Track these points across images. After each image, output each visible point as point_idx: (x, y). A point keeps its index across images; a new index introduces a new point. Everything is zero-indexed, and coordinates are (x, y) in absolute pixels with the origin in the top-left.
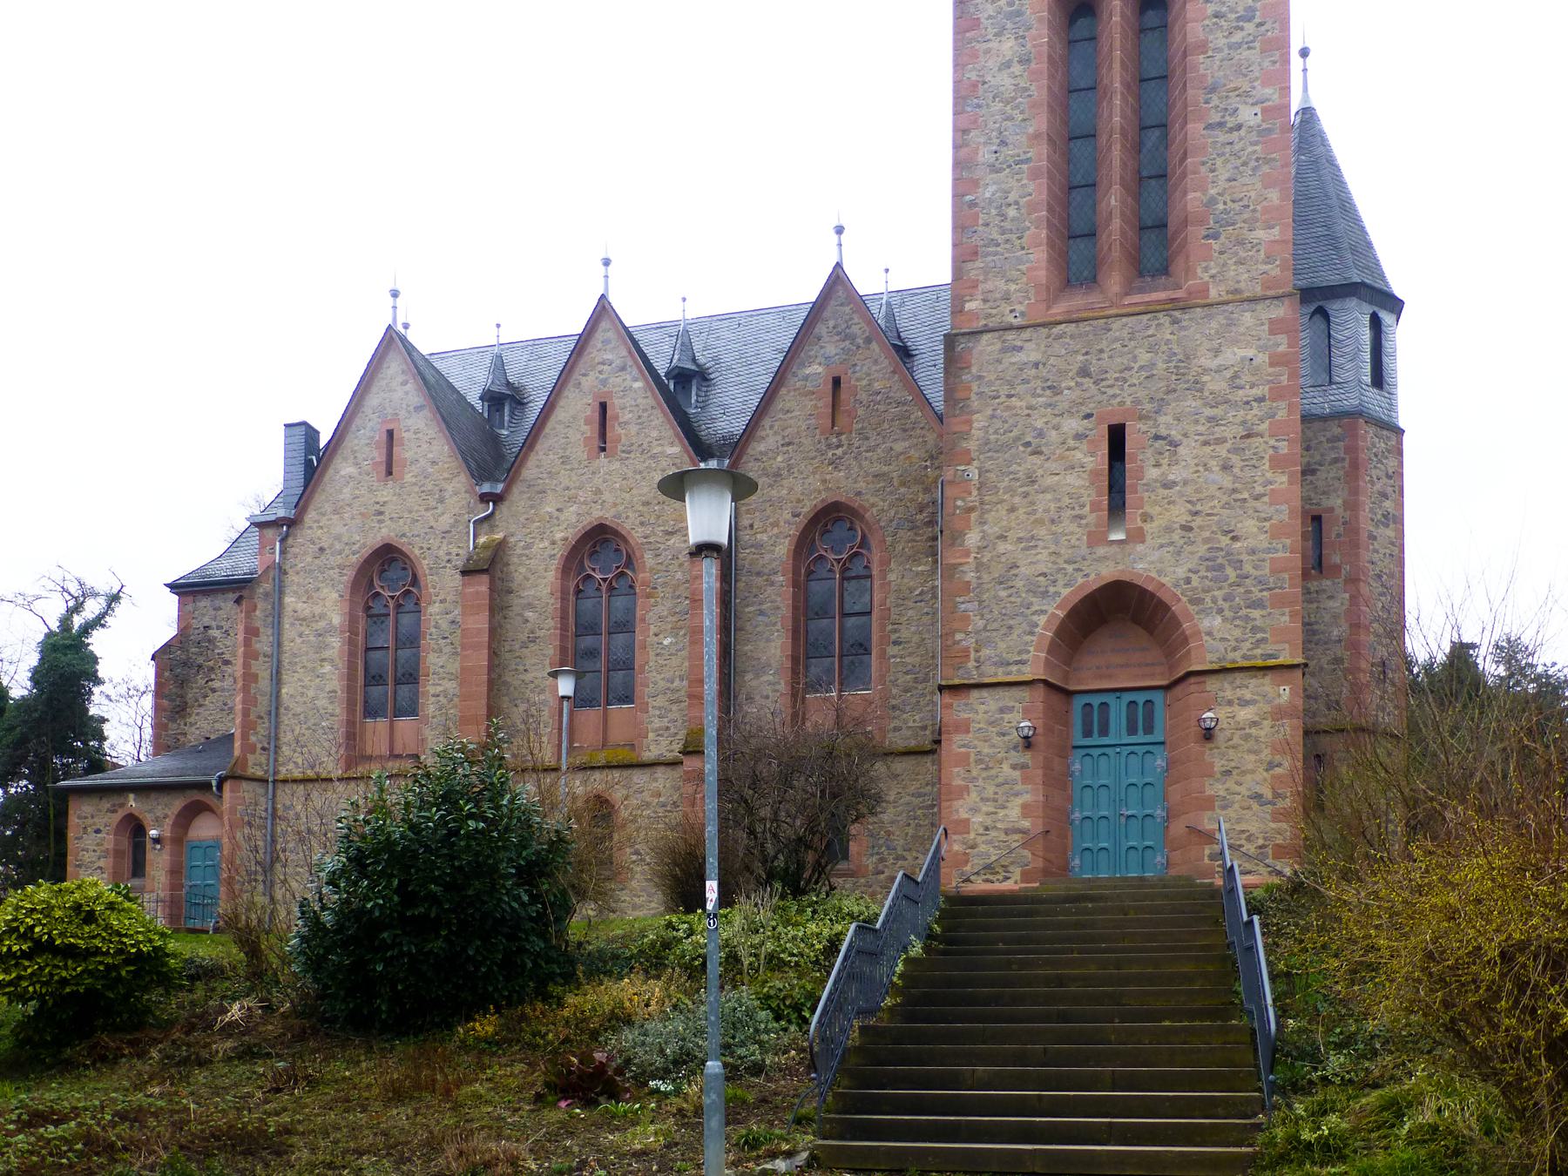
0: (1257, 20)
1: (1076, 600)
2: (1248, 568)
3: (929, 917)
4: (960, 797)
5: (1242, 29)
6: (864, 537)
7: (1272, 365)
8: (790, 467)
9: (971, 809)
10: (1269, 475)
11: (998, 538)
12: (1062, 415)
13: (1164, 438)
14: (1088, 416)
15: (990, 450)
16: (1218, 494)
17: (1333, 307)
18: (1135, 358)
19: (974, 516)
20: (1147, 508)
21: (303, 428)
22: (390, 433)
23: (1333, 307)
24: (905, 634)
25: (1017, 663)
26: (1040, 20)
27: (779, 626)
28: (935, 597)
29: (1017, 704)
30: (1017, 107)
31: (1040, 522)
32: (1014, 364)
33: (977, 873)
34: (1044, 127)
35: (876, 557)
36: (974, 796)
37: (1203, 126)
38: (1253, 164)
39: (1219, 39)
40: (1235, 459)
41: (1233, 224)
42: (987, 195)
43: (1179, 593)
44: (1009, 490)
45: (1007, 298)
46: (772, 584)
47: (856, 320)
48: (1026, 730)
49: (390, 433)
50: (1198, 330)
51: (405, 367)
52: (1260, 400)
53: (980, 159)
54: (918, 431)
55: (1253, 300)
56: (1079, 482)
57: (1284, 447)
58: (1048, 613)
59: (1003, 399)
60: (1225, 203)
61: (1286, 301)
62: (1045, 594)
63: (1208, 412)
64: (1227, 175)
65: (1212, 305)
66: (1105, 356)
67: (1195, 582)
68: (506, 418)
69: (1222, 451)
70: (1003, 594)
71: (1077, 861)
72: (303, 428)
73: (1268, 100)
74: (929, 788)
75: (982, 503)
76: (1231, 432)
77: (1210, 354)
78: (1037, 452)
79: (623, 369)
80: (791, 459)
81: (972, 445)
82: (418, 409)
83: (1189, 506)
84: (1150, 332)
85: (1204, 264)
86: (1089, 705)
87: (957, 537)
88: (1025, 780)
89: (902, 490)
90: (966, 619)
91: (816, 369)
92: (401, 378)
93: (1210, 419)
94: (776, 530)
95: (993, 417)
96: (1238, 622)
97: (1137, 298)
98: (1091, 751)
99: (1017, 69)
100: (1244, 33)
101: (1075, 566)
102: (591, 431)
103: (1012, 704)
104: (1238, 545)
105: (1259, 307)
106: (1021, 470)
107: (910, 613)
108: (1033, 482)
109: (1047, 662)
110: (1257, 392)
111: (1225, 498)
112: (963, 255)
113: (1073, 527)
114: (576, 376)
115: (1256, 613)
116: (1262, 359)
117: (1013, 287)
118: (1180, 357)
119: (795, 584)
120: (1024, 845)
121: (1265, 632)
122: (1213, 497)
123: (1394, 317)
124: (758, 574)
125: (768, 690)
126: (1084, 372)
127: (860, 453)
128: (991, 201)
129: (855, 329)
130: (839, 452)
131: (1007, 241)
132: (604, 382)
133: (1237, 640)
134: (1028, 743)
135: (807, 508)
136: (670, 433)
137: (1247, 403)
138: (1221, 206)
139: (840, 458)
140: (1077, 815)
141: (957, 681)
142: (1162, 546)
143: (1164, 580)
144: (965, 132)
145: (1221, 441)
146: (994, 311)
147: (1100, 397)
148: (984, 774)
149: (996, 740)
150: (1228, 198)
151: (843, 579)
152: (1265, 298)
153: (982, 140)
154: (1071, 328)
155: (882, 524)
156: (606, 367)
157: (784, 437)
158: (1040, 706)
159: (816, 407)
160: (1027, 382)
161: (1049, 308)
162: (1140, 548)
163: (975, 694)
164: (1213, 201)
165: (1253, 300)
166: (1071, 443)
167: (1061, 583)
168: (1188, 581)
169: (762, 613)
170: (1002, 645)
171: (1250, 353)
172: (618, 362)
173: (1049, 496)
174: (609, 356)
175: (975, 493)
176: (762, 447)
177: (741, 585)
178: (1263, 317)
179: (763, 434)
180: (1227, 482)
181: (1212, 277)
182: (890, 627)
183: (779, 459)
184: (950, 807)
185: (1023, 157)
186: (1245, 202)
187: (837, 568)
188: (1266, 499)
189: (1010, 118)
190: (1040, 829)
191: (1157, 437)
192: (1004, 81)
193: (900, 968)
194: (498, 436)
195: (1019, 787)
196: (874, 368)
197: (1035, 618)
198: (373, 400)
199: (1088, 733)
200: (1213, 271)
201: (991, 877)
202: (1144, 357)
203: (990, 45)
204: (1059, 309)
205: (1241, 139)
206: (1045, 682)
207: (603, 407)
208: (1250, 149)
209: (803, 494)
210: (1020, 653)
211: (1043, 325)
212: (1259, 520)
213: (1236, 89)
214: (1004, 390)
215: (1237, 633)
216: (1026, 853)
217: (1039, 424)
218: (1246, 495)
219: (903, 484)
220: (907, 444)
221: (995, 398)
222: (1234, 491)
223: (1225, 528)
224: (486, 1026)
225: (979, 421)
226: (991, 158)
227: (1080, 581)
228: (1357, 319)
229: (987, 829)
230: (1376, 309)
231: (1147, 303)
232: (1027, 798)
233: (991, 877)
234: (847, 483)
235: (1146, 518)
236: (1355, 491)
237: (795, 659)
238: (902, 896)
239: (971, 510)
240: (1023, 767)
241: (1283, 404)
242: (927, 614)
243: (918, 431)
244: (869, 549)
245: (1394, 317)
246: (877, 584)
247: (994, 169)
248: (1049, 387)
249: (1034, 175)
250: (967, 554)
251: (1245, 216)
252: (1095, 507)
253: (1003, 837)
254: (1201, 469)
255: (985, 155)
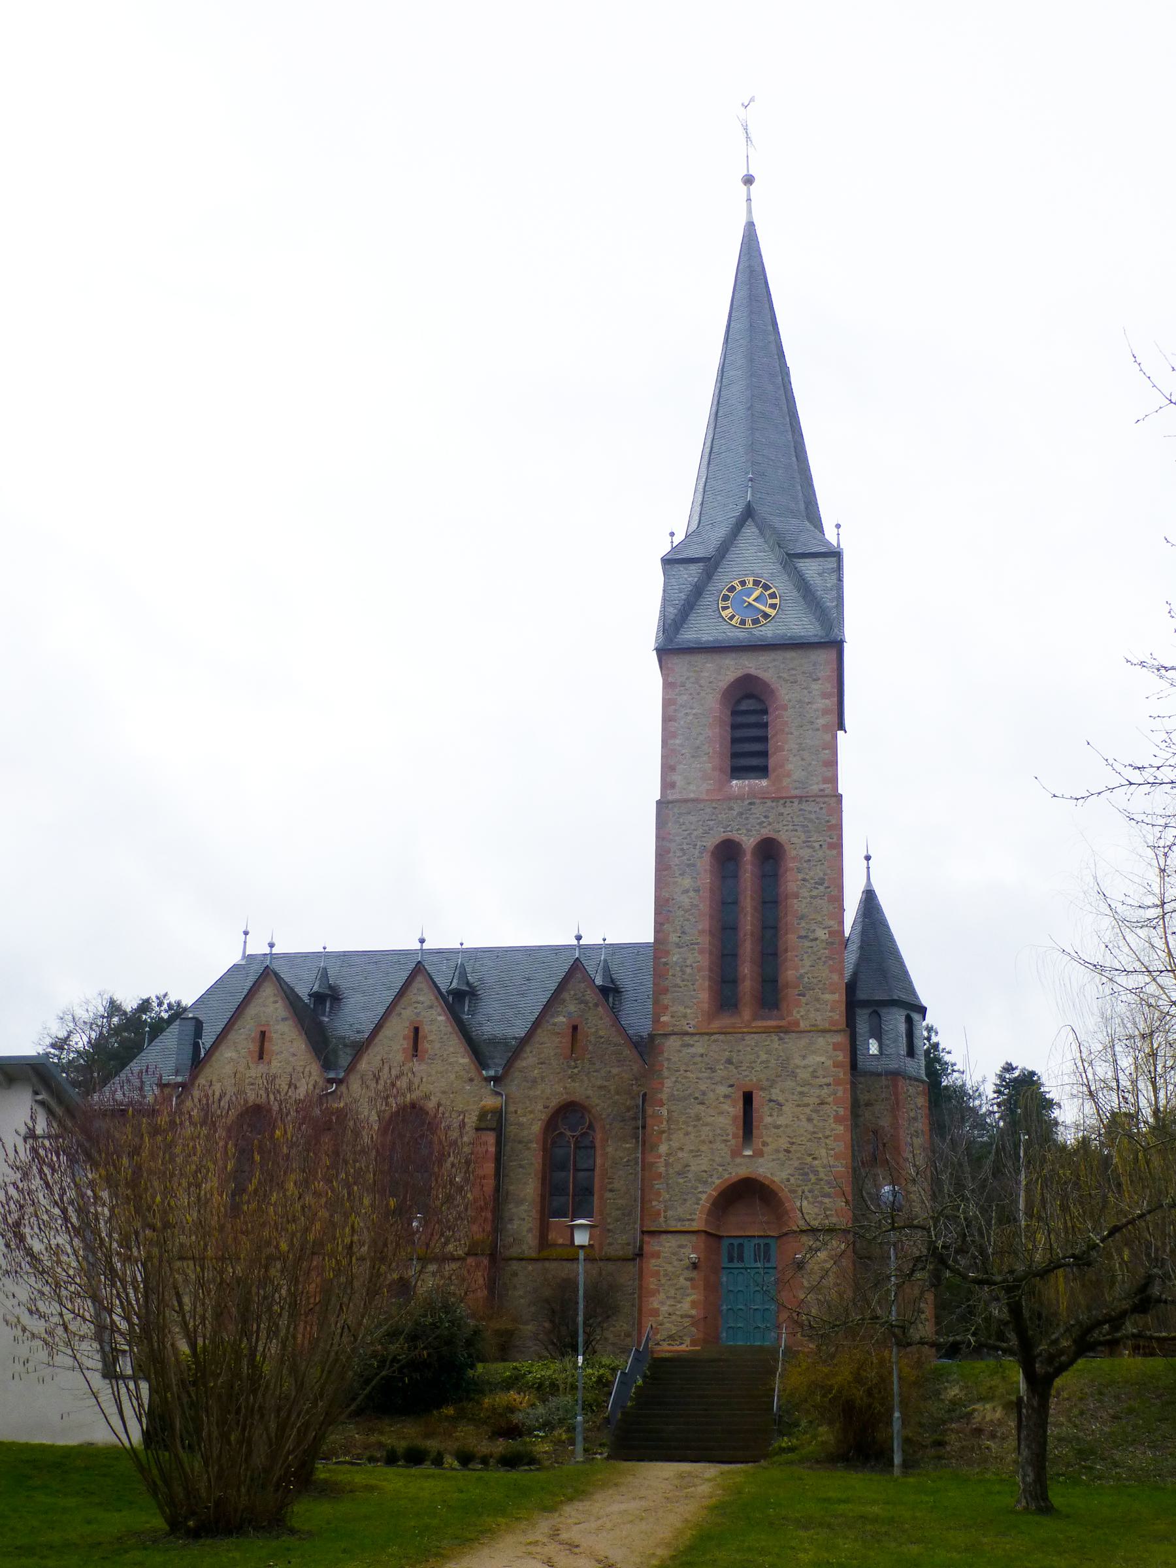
0: (826, 885)
1: (723, 1187)
2: (822, 1175)
3: (645, 1368)
4: (653, 1295)
5: (818, 889)
6: (590, 1123)
7: (834, 1067)
8: (543, 1078)
9: (660, 1303)
10: (833, 1125)
11: (679, 1149)
12: (716, 1084)
13: (774, 1101)
14: (731, 1086)
15: (674, 1100)
16: (805, 1134)
17: (883, 1011)
18: (758, 1057)
19: (664, 1135)
20: (765, 1139)
21: (194, 1021)
22: (263, 1034)
23: (883, 1011)
24: (616, 1185)
25: (689, 1220)
26: (705, 870)
27: (533, 1176)
28: (637, 1163)
29: (688, 1244)
30: (692, 914)
31: (703, 1142)
32: (688, 1053)
33: (664, 1340)
34: (707, 927)
35: (599, 1136)
36: (662, 1296)
37: (796, 936)
38: (823, 959)
39: (804, 892)
40: (814, 1115)
41: (813, 989)
42: (674, 959)
43: (783, 1187)
44: (685, 1123)
45: (685, 1016)
46: (529, 1149)
47: (588, 993)
48: (694, 1259)
49: (263, 1034)
50: (794, 1045)
51: (276, 992)
52: (828, 1085)
53: (671, 940)
54: (628, 1063)
55: (824, 1031)
56: (727, 1122)
57: (841, 1112)
58: (707, 1194)
59: (682, 1072)
60: (809, 978)
61: (842, 1033)
62: (705, 1182)
63: (799, 1089)
64: (809, 964)
65: (801, 1032)
66: (741, 1053)
67: (792, 1180)
68: (327, 1010)
69: (807, 1110)
70: (681, 1181)
71: (724, 1335)
72: (194, 1021)
73: (831, 927)
74: (631, 1282)
75: (669, 1129)
76: (813, 1100)
77: (800, 1058)
78: (702, 1103)
79: (431, 1007)
80: (543, 1072)
81: (664, 1096)
82: (284, 1019)
83: (789, 1139)
84: (767, 1043)
85: (797, 1009)
86: (732, 1244)
87: (654, 1147)
88: (693, 1288)
89: (617, 1097)
90: (658, 1194)
91: (561, 1019)
92: (272, 999)
93: (801, 1093)
94: (532, 1116)
95: (676, 1082)
96: (816, 1204)
97: (759, 1023)
98: (732, 1271)
99: (692, 894)
100: (818, 891)
101: (724, 1168)
102: (407, 1044)
103: (685, 1243)
104: (817, 1162)
105: (828, 1035)
106: (692, 1112)
107: (621, 1172)
108: (699, 1120)
109: (706, 1220)
110: (827, 1080)
111: (809, 1136)
112: (658, 930)
113: (723, 1146)
114: (398, 1008)
115: (826, 1200)
116: (829, 1063)
117: (689, 1011)
118: (784, 1058)
119: (544, 1150)
120: (692, 1325)
121: (832, 1211)
122: (802, 1135)
123: (921, 1016)
124: (520, 1142)
125: (524, 1215)
126: (729, 1061)
127: (589, 1073)
128: (676, 963)
129: (587, 997)
130: (576, 1071)
131: (686, 986)
132: (418, 1014)
133: (816, 1214)
134: (695, 1266)
135: (554, 1103)
136: (462, 1050)
137: (821, 1086)
138: (806, 979)
139: (577, 1074)
140: (724, 1307)
141: (652, 1229)
142: (773, 1160)
143: (775, 1179)
144: (662, 924)
145: (807, 1105)
146: (678, 1023)
147: (738, 1076)
148: (669, 1283)
149: (676, 1263)
150: (810, 975)
151: (577, 1147)
152: (830, 1031)
153: (671, 930)
154: (722, 1037)
155: (603, 1117)
156: (419, 1005)
157: (539, 1059)
158: (702, 1246)
159: (561, 1042)
160: (695, 1064)
161: (709, 1024)
162: (761, 1160)
163: (664, 1237)
164: (802, 976)
165: (824, 1031)
166: (722, 1099)
167: (715, 1176)
168: (788, 1180)
169: (521, 1166)
170: (679, 1210)
171: (823, 1059)
172: (428, 1003)
173: (708, 1128)
174: (421, 998)
175: (665, 1123)
176: (524, 1064)
177: (508, 1148)
178: (829, 1040)
179: (525, 1055)
180: (811, 1128)
181: (802, 1016)
182: (607, 1180)
183: (536, 1072)
184: (648, 1301)
185: (695, 941)
186: (820, 979)
187: (572, 1141)
188: (832, 1138)
189: (688, 920)
190: (702, 1316)
191: (771, 1101)
192: (685, 900)
193: (633, 1390)
194: (321, 1022)
195: (690, 1291)
196: (600, 1022)
197: (700, 1195)
198: (252, 1011)
199: (731, 1260)
200: (802, 1014)
201: (672, 1343)
202: (764, 1057)
203: (676, 880)
204: (716, 1025)
205: (817, 946)
206: (705, 1232)
207: (417, 1030)
208: (822, 951)
209: (550, 1094)
210: (691, 1214)
211: (707, 1034)
212: (827, 1149)
213: (814, 919)
214: (683, 1068)
215: (816, 1210)
216: (693, 1329)
217: (703, 1087)
218: (820, 1135)
219: (618, 1093)
220: (620, 1069)
221: (677, 1071)
222: (814, 1133)
223: (809, 1152)
224: (450, 1411)
225: (668, 1083)
226: (677, 940)
227: (726, 1176)
228: (896, 1019)
229: (670, 1314)
230: (908, 1012)
231: (765, 1027)
232: (693, 1297)
233: (672, 1343)
234: (581, 1090)
235: (765, 1144)
236: (895, 1117)
237: (543, 1197)
238: (635, 1359)
239: (663, 1132)
240: (691, 1279)
241: (841, 1088)
242: (631, 1174)
243: (628, 1063)
244: (594, 1131)
245: (921, 1016)
246: (599, 1152)
247: (678, 946)
248: (709, 1068)
249: (701, 952)
250: (660, 1157)
251: (820, 986)
252: (735, 1136)
253: (679, 1319)
254: (795, 1119)
255: (674, 938)
